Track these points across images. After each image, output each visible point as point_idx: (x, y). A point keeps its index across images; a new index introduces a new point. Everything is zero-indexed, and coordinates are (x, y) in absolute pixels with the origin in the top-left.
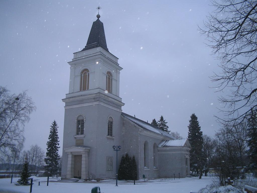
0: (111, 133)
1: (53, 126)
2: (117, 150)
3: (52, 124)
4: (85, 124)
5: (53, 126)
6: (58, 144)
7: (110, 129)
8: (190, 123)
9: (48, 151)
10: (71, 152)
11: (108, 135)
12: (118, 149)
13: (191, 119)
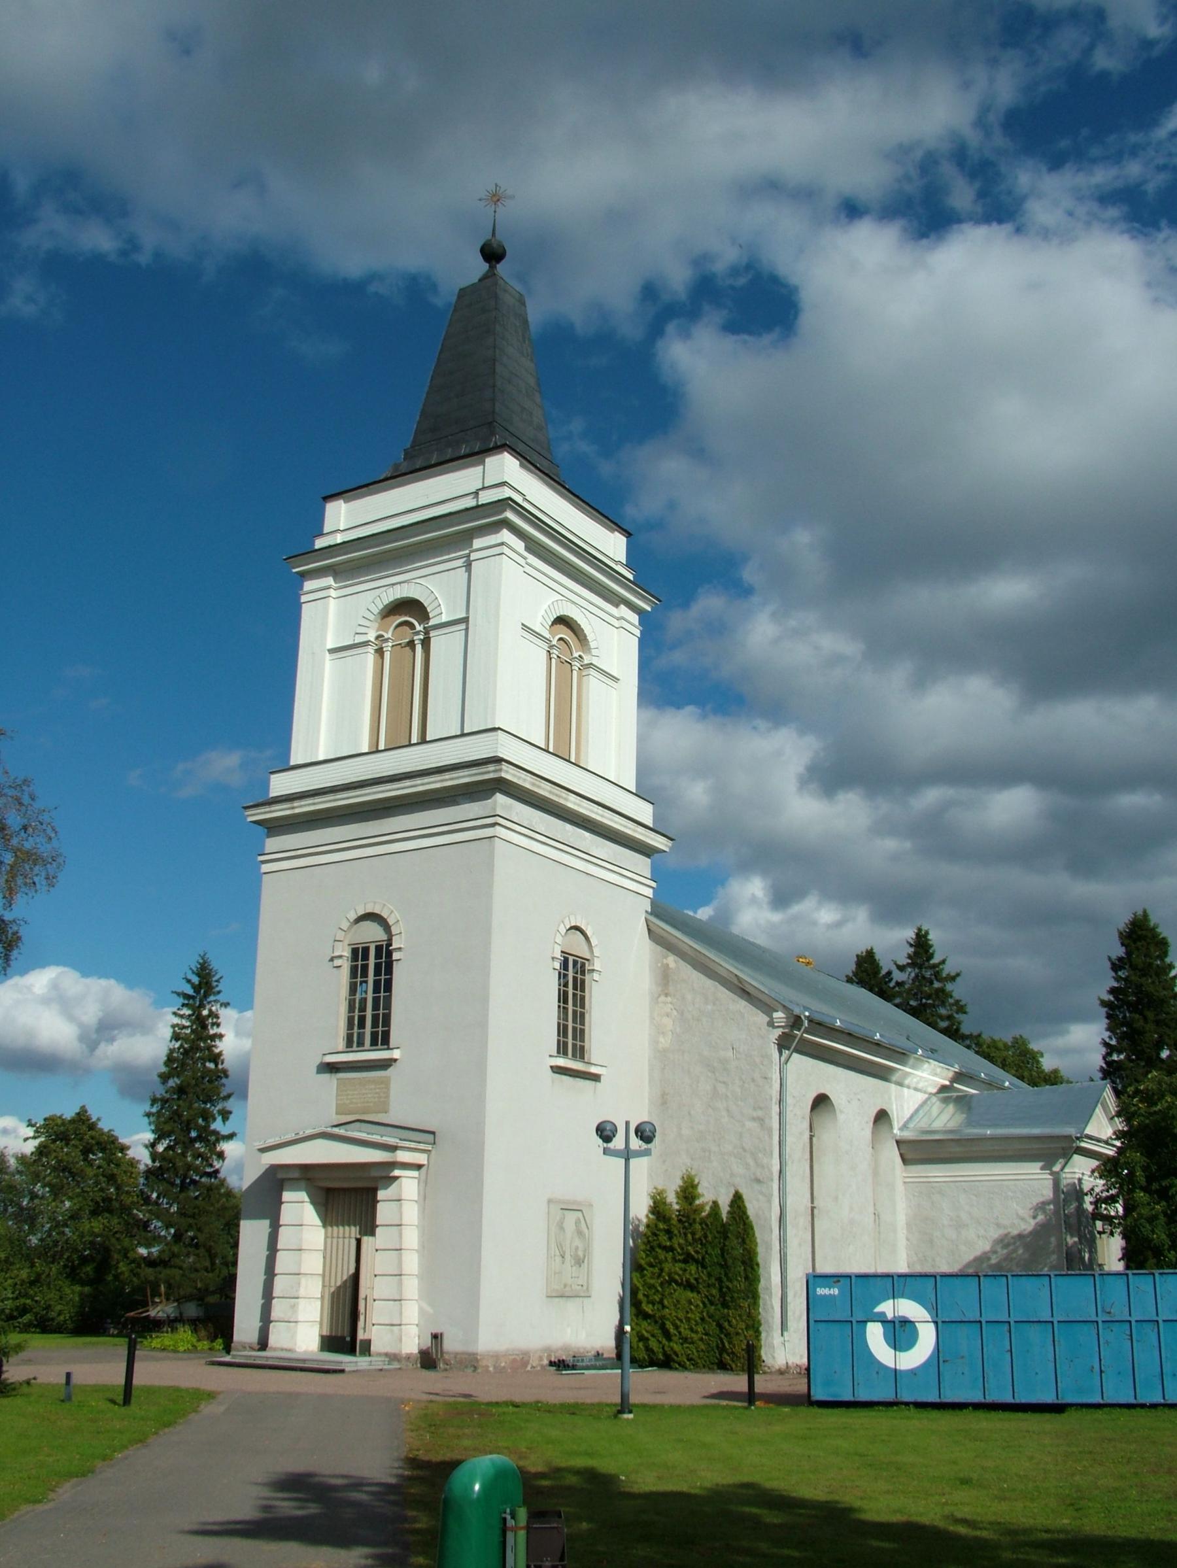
0: (580, 1034)
1: (190, 992)
2: (627, 1155)
3: (189, 981)
4: (397, 969)
5: (190, 992)
6: (226, 1115)
7: (570, 1024)
8: (1118, 979)
9: (154, 1156)
10: (306, 1168)
11: (562, 1049)
12: (636, 1143)
13: (1119, 951)
